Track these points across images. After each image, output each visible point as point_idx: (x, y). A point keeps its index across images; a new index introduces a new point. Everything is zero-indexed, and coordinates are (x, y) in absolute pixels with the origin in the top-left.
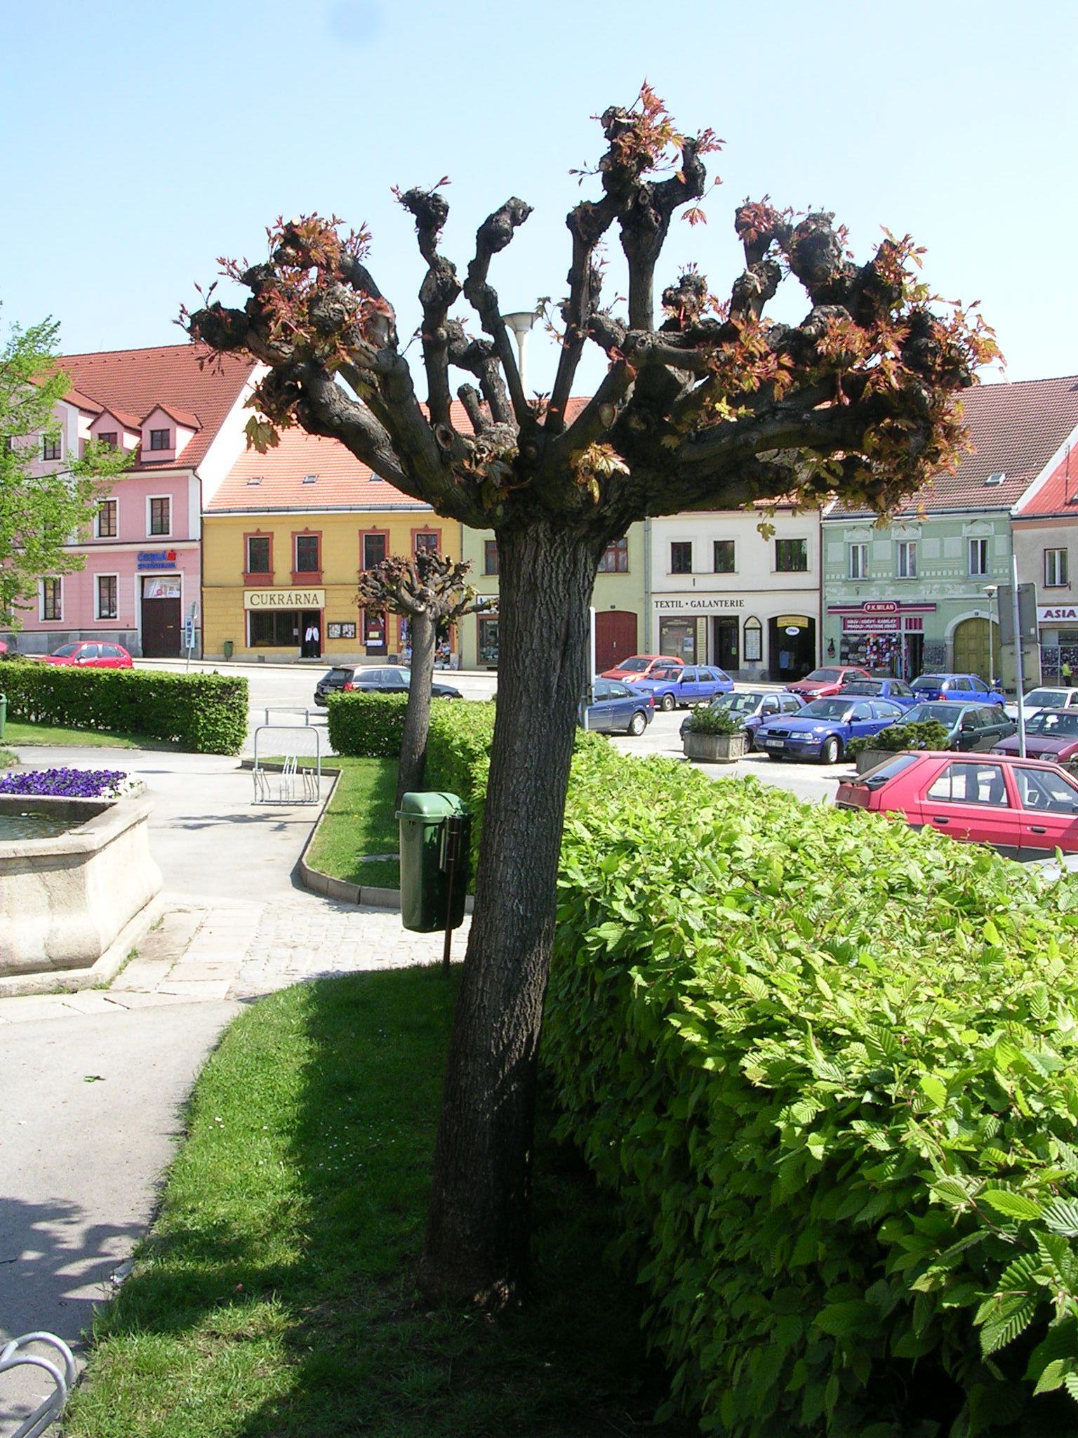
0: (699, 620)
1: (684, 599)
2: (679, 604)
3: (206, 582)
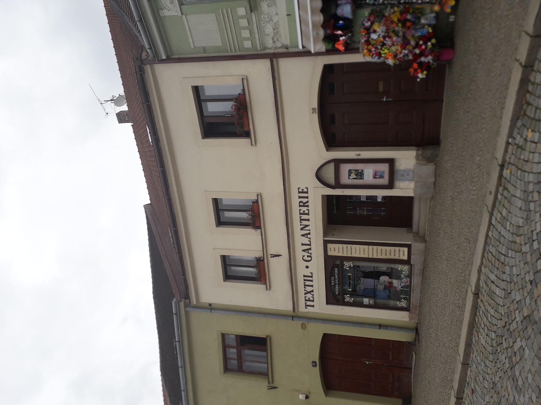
0: (330, 253)
1: (301, 271)
2: (308, 278)
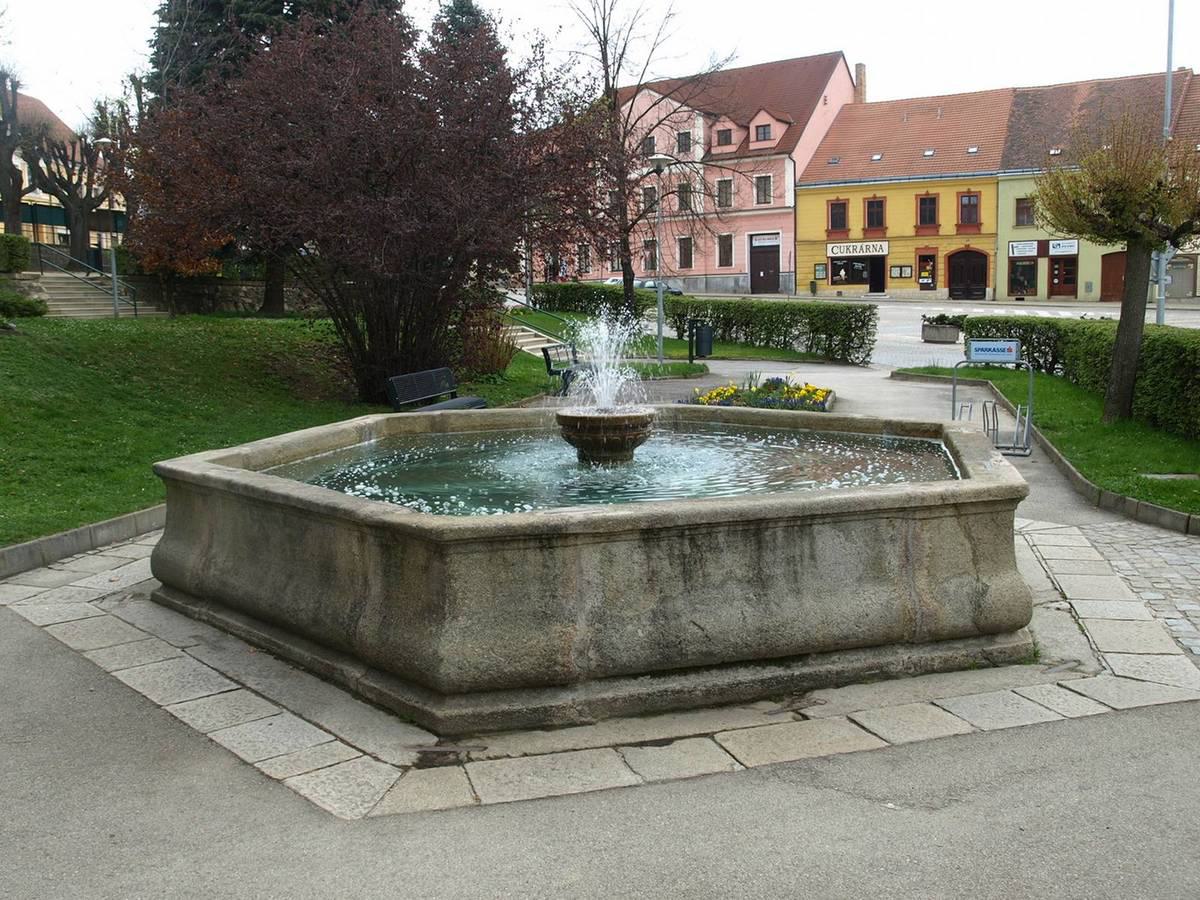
3: (799, 238)
